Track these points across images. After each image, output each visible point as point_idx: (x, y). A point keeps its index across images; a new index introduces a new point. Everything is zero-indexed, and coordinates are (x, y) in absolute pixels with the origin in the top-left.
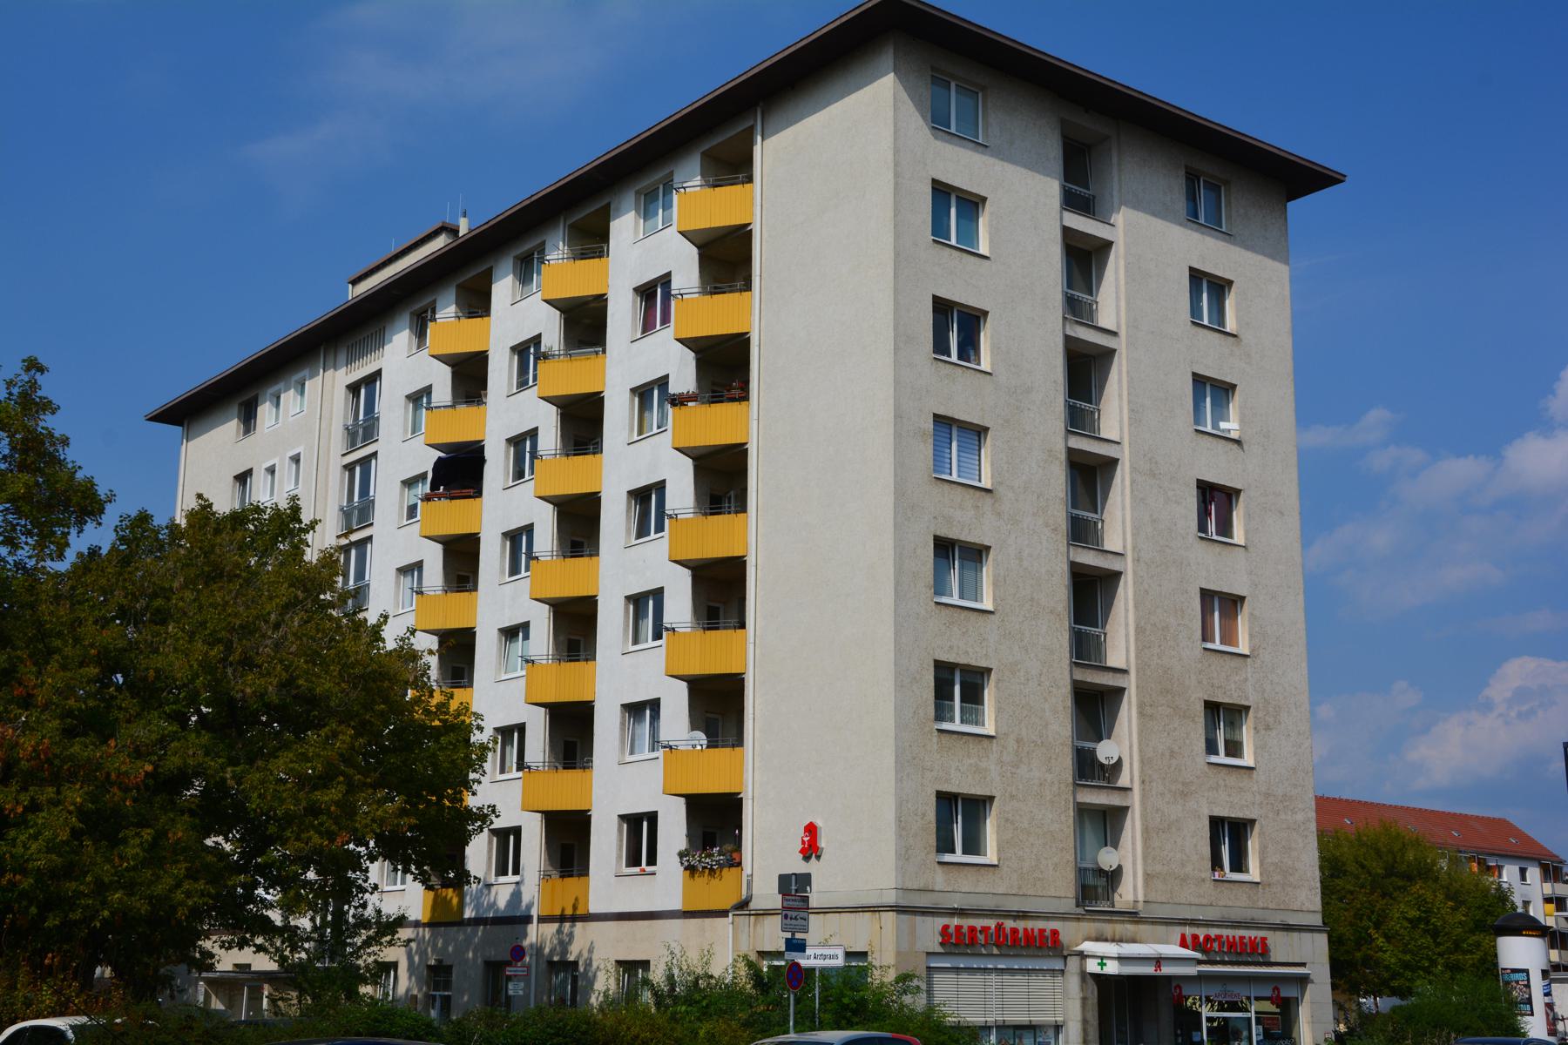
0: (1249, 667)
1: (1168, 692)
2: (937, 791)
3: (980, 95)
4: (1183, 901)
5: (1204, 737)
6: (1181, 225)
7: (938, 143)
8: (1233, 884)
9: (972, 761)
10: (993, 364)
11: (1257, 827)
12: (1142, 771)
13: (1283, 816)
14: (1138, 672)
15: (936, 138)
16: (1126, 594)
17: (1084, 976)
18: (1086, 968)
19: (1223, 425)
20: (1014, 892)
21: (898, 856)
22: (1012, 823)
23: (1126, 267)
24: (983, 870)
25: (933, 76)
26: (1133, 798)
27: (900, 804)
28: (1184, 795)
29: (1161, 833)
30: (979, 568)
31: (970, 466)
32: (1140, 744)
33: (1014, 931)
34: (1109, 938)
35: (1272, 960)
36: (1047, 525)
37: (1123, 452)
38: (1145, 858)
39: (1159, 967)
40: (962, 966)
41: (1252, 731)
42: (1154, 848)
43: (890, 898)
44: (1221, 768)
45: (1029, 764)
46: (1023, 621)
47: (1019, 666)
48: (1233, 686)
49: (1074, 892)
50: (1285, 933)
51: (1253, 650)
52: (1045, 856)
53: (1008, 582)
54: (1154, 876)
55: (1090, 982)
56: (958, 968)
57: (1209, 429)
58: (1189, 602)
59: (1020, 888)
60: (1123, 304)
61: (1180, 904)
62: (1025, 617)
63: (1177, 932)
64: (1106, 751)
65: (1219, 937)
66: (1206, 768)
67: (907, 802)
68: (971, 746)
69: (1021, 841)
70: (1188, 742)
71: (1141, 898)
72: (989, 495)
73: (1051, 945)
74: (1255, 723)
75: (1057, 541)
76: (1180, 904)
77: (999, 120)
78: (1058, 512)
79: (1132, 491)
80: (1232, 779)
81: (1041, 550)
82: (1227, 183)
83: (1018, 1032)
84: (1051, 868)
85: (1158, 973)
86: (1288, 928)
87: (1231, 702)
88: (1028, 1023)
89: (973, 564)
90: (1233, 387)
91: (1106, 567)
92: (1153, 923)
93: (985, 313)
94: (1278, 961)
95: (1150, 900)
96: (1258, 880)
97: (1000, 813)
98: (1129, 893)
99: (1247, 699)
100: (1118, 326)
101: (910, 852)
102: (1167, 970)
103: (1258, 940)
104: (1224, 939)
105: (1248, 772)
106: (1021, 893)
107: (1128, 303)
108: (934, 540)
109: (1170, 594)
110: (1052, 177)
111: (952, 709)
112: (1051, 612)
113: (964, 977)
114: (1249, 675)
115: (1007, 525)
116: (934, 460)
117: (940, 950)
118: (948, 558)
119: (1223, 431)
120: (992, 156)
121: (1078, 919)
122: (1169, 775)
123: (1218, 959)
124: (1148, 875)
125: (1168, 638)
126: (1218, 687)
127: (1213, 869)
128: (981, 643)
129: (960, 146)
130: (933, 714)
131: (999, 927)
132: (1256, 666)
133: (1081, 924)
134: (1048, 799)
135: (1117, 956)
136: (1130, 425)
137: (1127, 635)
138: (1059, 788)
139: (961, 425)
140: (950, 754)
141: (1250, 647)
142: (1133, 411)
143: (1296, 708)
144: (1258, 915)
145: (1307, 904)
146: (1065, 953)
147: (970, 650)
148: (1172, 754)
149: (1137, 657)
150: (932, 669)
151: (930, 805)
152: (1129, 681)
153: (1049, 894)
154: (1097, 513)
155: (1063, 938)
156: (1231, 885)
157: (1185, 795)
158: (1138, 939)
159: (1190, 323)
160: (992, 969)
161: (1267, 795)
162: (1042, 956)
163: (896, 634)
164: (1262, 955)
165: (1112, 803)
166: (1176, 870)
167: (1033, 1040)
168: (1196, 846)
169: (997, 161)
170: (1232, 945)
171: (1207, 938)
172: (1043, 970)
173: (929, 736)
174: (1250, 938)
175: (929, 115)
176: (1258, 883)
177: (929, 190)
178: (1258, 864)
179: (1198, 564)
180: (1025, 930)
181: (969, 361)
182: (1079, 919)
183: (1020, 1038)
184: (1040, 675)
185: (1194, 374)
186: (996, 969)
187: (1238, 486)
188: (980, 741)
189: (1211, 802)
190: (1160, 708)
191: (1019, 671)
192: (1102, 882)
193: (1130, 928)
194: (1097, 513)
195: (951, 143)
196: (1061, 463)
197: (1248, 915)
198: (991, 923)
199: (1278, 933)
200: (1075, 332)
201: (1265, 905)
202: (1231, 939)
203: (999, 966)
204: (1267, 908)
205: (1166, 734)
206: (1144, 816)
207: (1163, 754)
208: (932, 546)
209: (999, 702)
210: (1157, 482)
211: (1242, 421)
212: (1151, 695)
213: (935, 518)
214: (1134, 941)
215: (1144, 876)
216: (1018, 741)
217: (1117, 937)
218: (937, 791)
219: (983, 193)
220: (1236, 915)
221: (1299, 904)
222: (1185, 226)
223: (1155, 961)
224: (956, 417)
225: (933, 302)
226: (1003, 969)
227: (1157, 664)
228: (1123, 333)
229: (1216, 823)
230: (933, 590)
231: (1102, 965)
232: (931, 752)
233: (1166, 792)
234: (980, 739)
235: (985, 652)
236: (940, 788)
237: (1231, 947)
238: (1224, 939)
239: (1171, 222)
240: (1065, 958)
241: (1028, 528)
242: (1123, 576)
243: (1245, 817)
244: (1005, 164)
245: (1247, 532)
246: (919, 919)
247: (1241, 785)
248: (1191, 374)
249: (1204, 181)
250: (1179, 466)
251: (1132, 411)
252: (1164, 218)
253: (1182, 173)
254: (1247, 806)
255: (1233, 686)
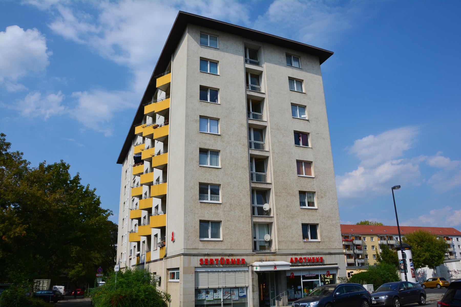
0: (315, 181)
1: (285, 189)
2: (200, 220)
3: (218, 38)
4: (293, 248)
5: (299, 201)
6: (285, 66)
7: (202, 49)
8: (311, 242)
9: (213, 211)
10: (221, 102)
11: (319, 226)
12: (277, 211)
13: (328, 222)
14: (274, 183)
15: (201, 47)
16: (270, 162)
17: (253, 272)
18: (253, 270)
19: (302, 116)
20: (229, 248)
21: (185, 239)
22: (228, 228)
23: (267, 77)
24: (217, 242)
25: (200, 34)
26: (274, 220)
27: (186, 224)
28: (292, 218)
29: (284, 229)
30: (217, 157)
31: (203, 125)
32: (276, 204)
33: (228, 260)
34: (264, 260)
35: (325, 264)
36: (240, 144)
37: (268, 124)
38: (278, 237)
39: (276, 268)
40: (209, 271)
41: (316, 199)
42: (281, 234)
43: (182, 252)
44: (306, 210)
45: (235, 211)
46: (232, 171)
47: (230, 183)
48: (309, 186)
49: (252, 247)
50: (330, 256)
51: (315, 176)
52: (240, 237)
53: (226, 160)
54: (281, 242)
55: (255, 274)
56: (208, 271)
57: (299, 117)
58: (292, 164)
59: (231, 247)
60: (266, 86)
61: (291, 249)
62: (233, 169)
63: (289, 258)
64: (266, 207)
65: (305, 258)
66: (300, 210)
67: (188, 223)
68: (213, 206)
69: (232, 234)
70: (293, 203)
71: (277, 248)
72: (220, 136)
73: (243, 263)
74: (317, 196)
75: (244, 148)
76: (291, 249)
77: (222, 42)
78: (244, 140)
79: (271, 134)
80: (310, 212)
81: (239, 151)
82: (300, 57)
83: (232, 290)
84: (243, 241)
85: (275, 270)
86: (330, 254)
87: (308, 191)
88: (235, 287)
89: (216, 156)
90: (306, 106)
91: (263, 155)
92: (281, 255)
93: (219, 89)
94: (327, 264)
95: (280, 248)
96: (320, 241)
97: (224, 226)
98: (274, 247)
99: (315, 190)
100: (265, 91)
101: (189, 238)
102: (278, 269)
103: (319, 258)
104: (307, 258)
105: (315, 210)
106: (231, 249)
107: (268, 86)
108: (200, 149)
109: (285, 161)
110: (241, 56)
111: (208, 196)
112: (242, 168)
113: (211, 274)
114: (315, 183)
115: (226, 144)
116: (200, 128)
117: (200, 266)
118: (207, 155)
119: (303, 118)
120: (220, 51)
121: (253, 255)
122: (286, 212)
123: (305, 264)
124: (279, 241)
125: (285, 174)
126: (304, 187)
127: (304, 238)
128: (216, 177)
129: (210, 49)
130: (199, 198)
131: (222, 259)
132: (317, 180)
133: (254, 257)
134: (242, 221)
135: (258, 265)
136: (270, 117)
137: (271, 174)
138: (246, 217)
139: (211, 118)
140: (205, 209)
141: (315, 175)
142: (271, 113)
143: (332, 192)
144: (320, 251)
145: (337, 247)
146: (248, 265)
147: (213, 179)
148: (288, 206)
149: (274, 179)
150: (198, 185)
151: (197, 224)
152: (272, 186)
153: (242, 248)
154: (263, 142)
155: (246, 260)
156: (310, 243)
157: (293, 218)
158: (276, 260)
159: (289, 90)
160: (221, 271)
161: (322, 216)
162: (240, 267)
163: (185, 175)
164: (321, 262)
165: (266, 221)
166: (290, 240)
167: (238, 291)
168: (297, 232)
169: (222, 52)
170: (309, 260)
171: (301, 259)
172: (238, 271)
173: (197, 204)
174: (316, 258)
175: (199, 42)
176: (320, 242)
177: (199, 59)
178: (320, 236)
179: (295, 153)
180: (232, 259)
181: (216, 102)
182: (253, 255)
183: (233, 291)
184: (239, 185)
185: (291, 103)
186: (223, 271)
187: (308, 132)
188: (216, 205)
189: (302, 220)
190: (283, 194)
191: (231, 184)
192: (267, 245)
193: (272, 257)
194: (263, 142)
195: (207, 49)
196: (245, 127)
197: (317, 251)
198: (219, 258)
199: (327, 256)
200: (251, 94)
201: (323, 248)
202: (309, 258)
203: (223, 270)
204: (323, 249)
205: (285, 201)
206: (277, 224)
207: (284, 207)
208: (199, 151)
209: (223, 194)
210: (280, 131)
211: (309, 115)
212: (279, 190)
213: (200, 143)
214: (274, 261)
215: (278, 242)
216: (230, 205)
217: (267, 260)
218: (200, 220)
219: (305, 105)
220: (312, 251)
221: (335, 247)
222: (287, 67)
223: (274, 267)
224: (208, 116)
225: (200, 87)
226: (225, 271)
227: (282, 181)
228: (267, 93)
229: (305, 226)
230: (199, 163)
231: (256, 268)
232: (198, 208)
233: (286, 217)
234: (216, 204)
235: (218, 180)
236: (201, 219)
237: (309, 261)
238: (307, 258)
239: (282, 66)
240: (248, 267)
241: (234, 145)
242: (269, 157)
243: (314, 223)
244: (225, 53)
245: (312, 144)
246: (192, 257)
247: (313, 214)
248: (290, 103)
249: (293, 57)
250: (287, 127)
251: (270, 113)
252: (280, 65)
253: (285, 54)
254: (315, 220)
255: (309, 186)
